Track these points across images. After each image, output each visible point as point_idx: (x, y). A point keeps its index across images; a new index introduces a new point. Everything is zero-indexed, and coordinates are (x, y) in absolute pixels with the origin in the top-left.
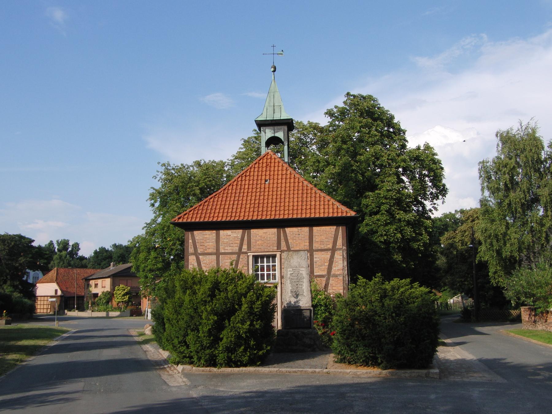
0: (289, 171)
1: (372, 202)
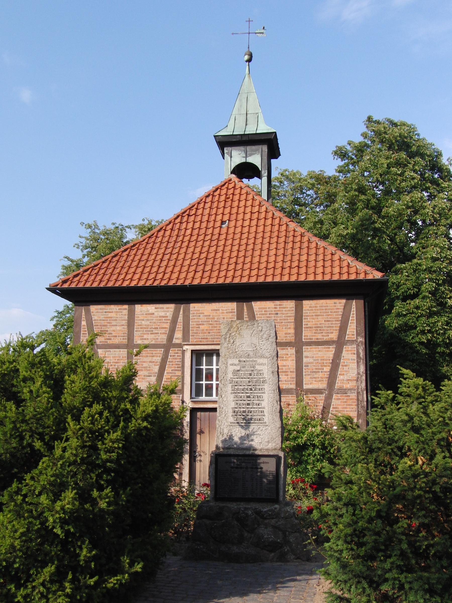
0: (264, 206)
1: (406, 280)
